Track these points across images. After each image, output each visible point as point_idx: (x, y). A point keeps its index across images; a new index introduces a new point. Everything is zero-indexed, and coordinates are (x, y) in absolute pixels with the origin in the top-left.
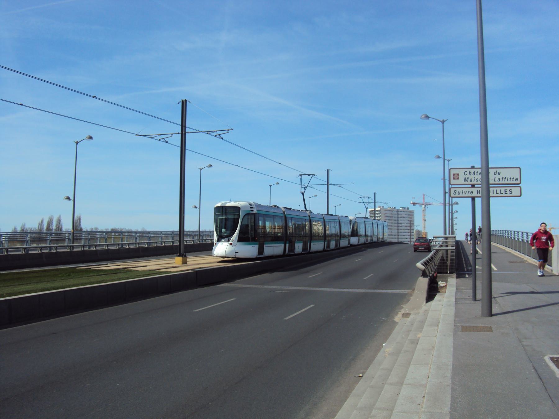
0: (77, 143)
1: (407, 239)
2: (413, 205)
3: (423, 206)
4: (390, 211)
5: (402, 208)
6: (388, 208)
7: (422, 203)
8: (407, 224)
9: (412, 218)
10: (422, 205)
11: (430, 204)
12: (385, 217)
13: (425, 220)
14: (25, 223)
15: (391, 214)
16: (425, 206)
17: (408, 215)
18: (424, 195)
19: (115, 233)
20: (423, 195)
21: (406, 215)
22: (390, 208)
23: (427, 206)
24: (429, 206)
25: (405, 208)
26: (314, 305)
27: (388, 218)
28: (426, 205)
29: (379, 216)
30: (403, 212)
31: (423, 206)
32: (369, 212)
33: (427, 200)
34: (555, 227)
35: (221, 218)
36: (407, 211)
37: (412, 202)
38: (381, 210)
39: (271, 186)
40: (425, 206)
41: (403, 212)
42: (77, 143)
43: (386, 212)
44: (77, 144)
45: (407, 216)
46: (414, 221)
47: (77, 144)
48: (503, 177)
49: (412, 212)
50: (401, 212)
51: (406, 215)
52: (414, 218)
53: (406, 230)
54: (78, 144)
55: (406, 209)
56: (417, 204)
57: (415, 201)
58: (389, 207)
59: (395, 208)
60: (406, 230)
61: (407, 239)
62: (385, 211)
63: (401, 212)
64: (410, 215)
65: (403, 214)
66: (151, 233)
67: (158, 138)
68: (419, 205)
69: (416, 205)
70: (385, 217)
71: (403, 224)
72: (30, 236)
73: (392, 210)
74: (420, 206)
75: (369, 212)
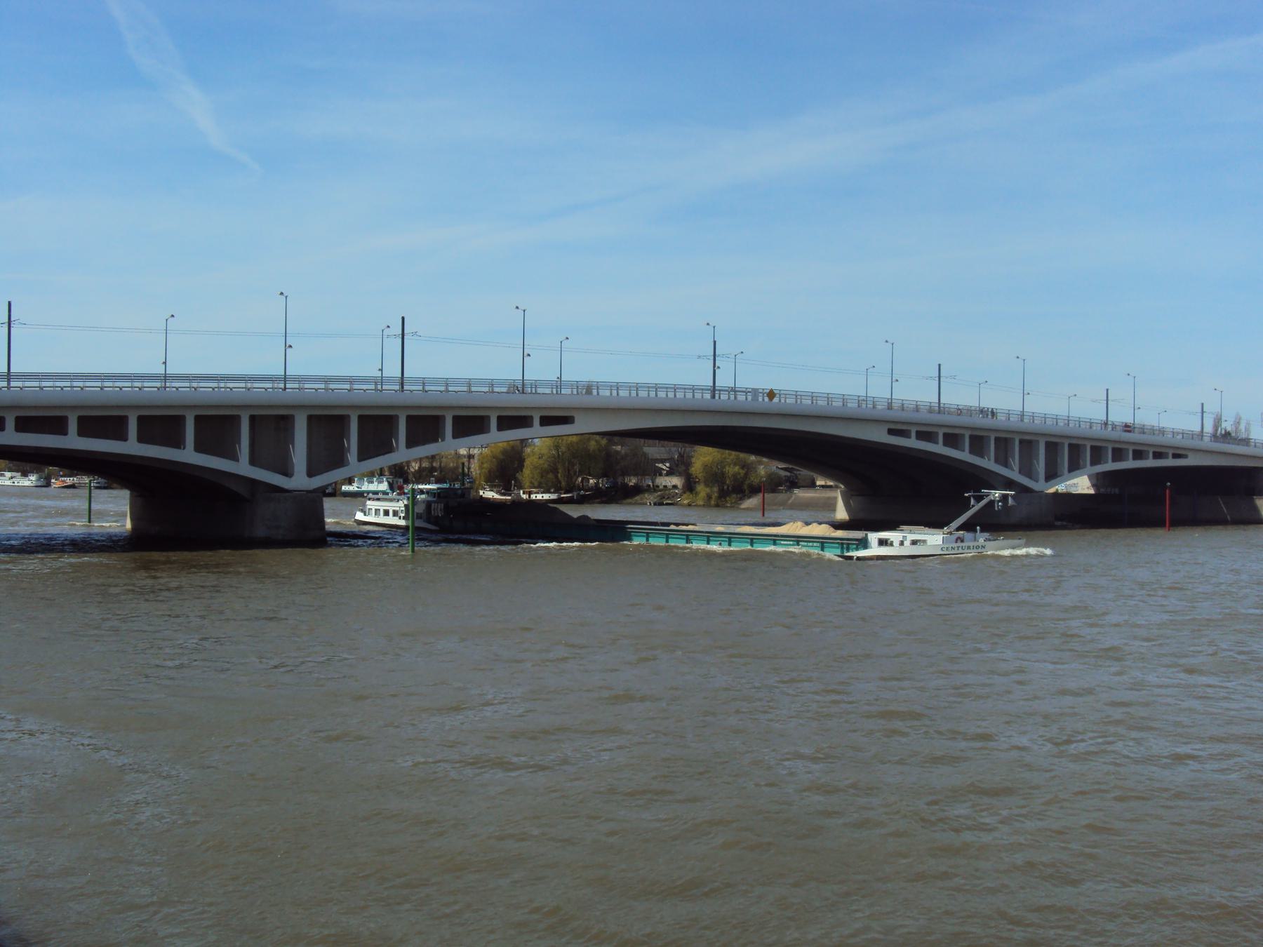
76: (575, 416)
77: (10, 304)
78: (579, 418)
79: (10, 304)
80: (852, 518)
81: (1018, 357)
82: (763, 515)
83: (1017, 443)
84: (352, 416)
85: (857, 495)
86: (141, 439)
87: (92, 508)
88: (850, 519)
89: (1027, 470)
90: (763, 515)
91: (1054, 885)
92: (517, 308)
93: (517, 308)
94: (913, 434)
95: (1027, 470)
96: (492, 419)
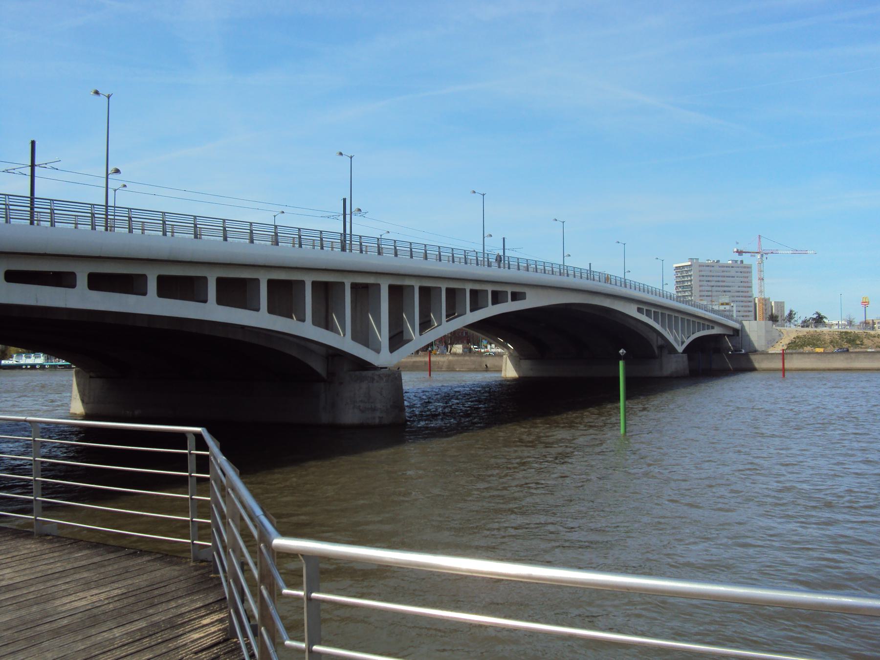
0: (275, 216)
3: (759, 256)
4: (708, 266)
6: (707, 262)
8: (739, 287)
9: (747, 277)
10: (756, 254)
11: (772, 253)
12: (700, 276)
14: (817, 313)
15: (711, 271)
16: (762, 255)
17: (741, 272)
18: (760, 238)
20: (758, 238)
21: (737, 272)
22: (709, 262)
23: (765, 256)
25: (736, 261)
27: (705, 278)
29: (690, 276)
30: (732, 267)
31: (759, 256)
32: (675, 270)
33: (766, 246)
36: (742, 265)
37: (735, 250)
38: (693, 266)
40: (762, 255)
41: (732, 267)
42: (275, 216)
43: (702, 268)
44: (109, 99)
45: (739, 274)
47: (109, 99)
49: (748, 267)
50: (729, 267)
51: (737, 272)
53: (737, 297)
54: (110, 98)
55: (739, 262)
56: (744, 252)
57: (740, 249)
58: (708, 260)
59: (718, 261)
60: (737, 297)
62: (700, 266)
63: (729, 267)
64: (745, 272)
65: (733, 272)
66: (631, 571)
67: (332, 217)
69: (744, 254)
70: (700, 276)
71: (732, 286)
73: (713, 265)
74: (751, 256)
75: (675, 270)
76: (526, 292)
77: (33, 143)
78: (529, 293)
79: (33, 143)
80: (521, 375)
81: (341, 154)
82: (784, 375)
83: (667, 315)
84: (209, 279)
85: (526, 359)
86: (220, 301)
87: (781, 361)
88: (519, 377)
89: (363, 335)
90: (784, 375)
91: (523, 523)
92: (97, 93)
93: (97, 93)
94: (152, 286)
95: (363, 335)
96: (467, 290)
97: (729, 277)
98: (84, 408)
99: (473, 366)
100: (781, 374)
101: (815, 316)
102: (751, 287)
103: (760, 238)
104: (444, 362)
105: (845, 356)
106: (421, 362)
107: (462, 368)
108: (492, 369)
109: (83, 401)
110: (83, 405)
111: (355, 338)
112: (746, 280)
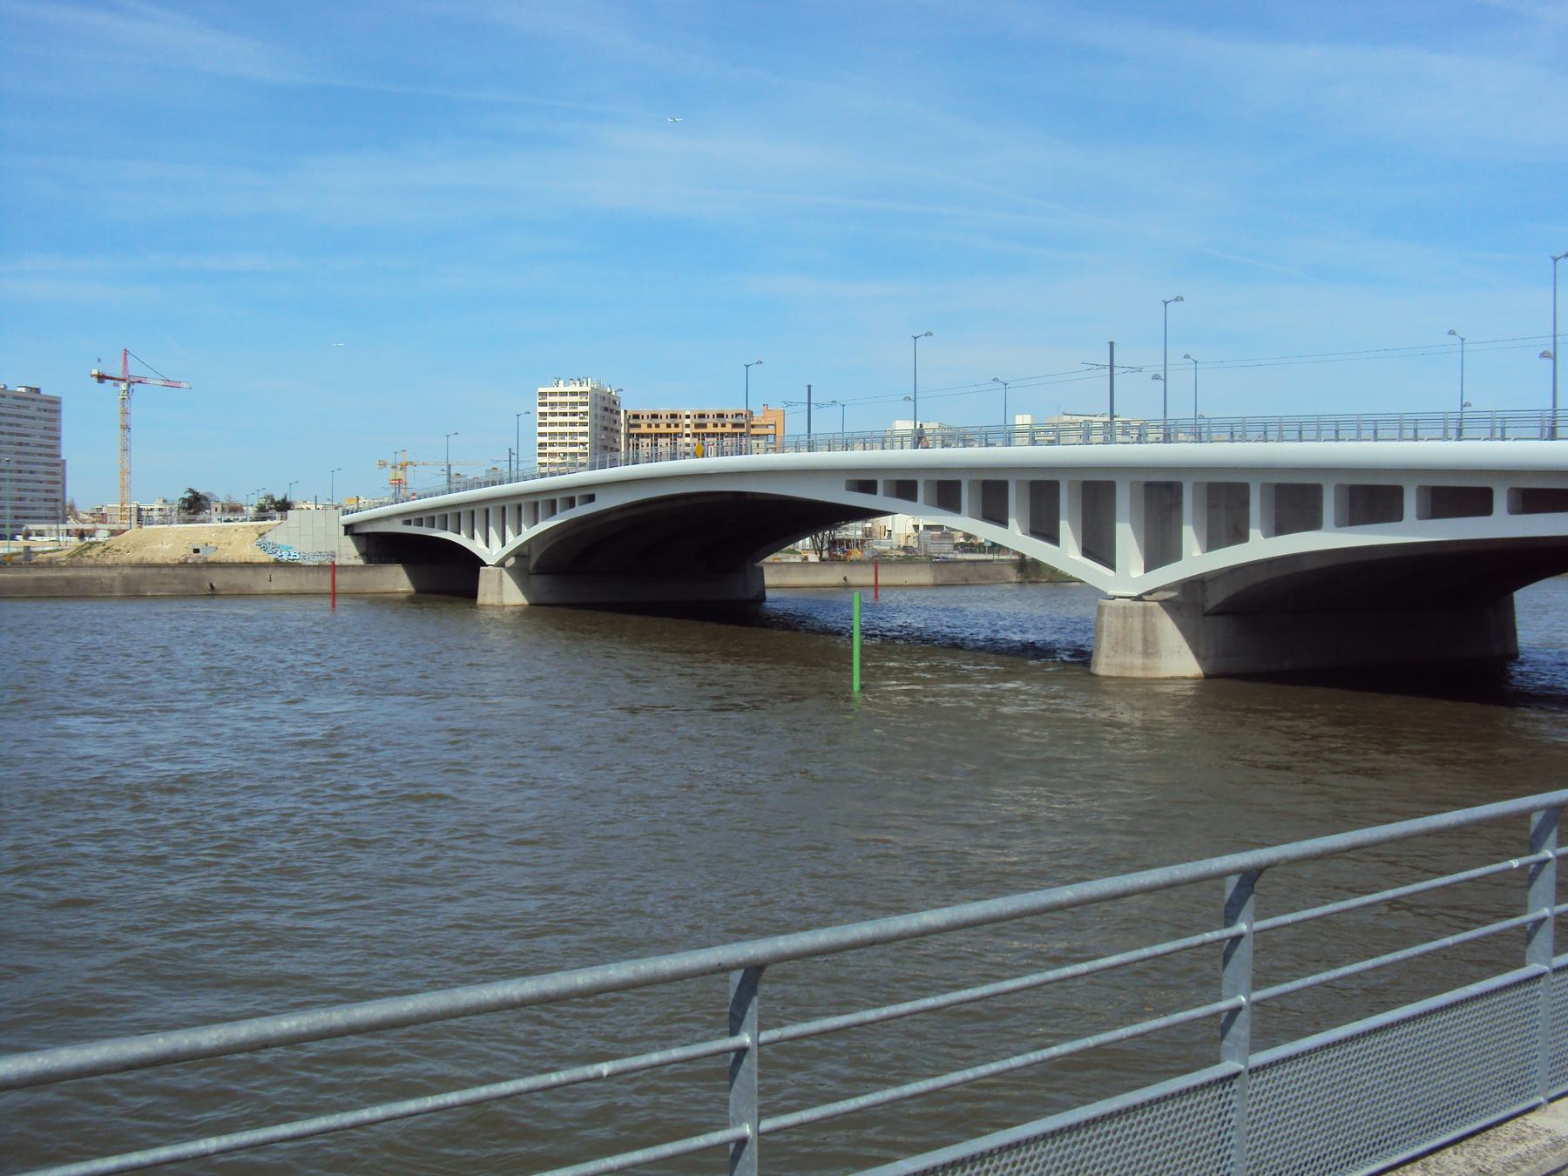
1: (41, 482)
2: (99, 382)
3: (123, 386)
5: (23, 390)
7: (121, 377)
11: (140, 382)
13: (126, 428)
14: (191, 490)
18: (126, 355)
19: (845, 560)
24: (136, 387)
26: (1556, 828)
28: (131, 382)
33: (135, 370)
34: (413, 460)
35: (622, 431)
37: (95, 372)
39: (915, 338)
46: (60, 431)
48: (1470, 405)
49: (51, 402)
52: (60, 419)
57: (103, 371)
61: (41, 482)
68: (113, 381)
72: (373, 786)
82: (334, 605)
89: (1099, 548)
90: (334, 605)
97: (26, 417)
98: (1202, 666)
99: (182, 587)
100: (328, 602)
101: (188, 495)
102: (58, 438)
103: (126, 355)
104: (113, 579)
105: (1051, 585)
106: (56, 579)
107: (159, 591)
108: (223, 592)
109: (1197, 655)
110: (1199, 662)
111: (1087, 552)
112: (50, 424)
